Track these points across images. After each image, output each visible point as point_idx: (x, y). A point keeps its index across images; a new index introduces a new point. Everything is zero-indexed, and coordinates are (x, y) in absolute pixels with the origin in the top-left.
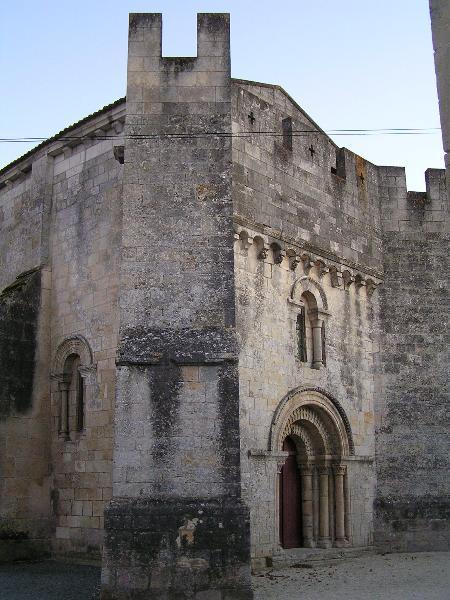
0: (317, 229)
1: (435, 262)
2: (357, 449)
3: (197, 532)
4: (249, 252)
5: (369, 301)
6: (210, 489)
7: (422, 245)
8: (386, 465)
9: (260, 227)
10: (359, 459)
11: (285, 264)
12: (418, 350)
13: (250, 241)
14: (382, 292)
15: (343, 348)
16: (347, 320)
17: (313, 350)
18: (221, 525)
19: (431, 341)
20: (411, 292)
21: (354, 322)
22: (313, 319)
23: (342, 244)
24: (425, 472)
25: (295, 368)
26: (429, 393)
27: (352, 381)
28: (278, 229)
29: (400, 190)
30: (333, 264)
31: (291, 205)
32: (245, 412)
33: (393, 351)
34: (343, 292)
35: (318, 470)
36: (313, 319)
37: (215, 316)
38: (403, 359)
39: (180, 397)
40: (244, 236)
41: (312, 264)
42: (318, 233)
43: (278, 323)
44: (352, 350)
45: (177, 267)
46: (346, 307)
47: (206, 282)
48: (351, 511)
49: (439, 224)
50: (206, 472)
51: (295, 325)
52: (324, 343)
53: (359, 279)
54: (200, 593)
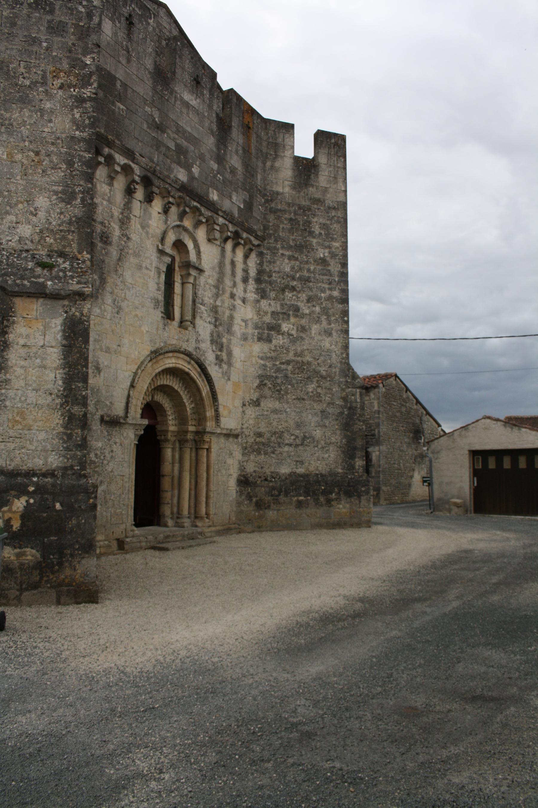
0: (195, 170)
1: (317, 229)
2: (223, 420)
3: (25, 516)
4: (116, 184)
5: (245, 263)
6: (46, 458)
7: (305, 210)
8: (251, 440)
9: (129, 154)
10: (224, 432)
11: (157, 205)
12: (292, 320)
13: (118, 169)
14: (261, 255)
15: (214, 310)
16: (220, 280)
17: (182, 307)
18: (58, 506)
19: (307, 311)
20: (290, 258)
21: (228, 282)
22: (184, 273)
23: (221, 194)
24: (291, 449)
25: (161, 326)
26: (301, 367)
27: (222, 347)
28: (152, 161)
29: (287, 147)
30: (209, 214)
31: (169, 136)
32: (98, 369)
33: (268, 319)
34: (220, 248)
35: (180, 441)
36: (184, 273)
37: (64, 238)
38: (275, 328)
39: (11, 337)
40: (110, 160)
41: (187, 210)
42: (196, 175)
43: (144, 271)
44: (224, 313)
45: (17, 170)
46: (221, 265)
47: (56, 193)
48: (212, 487)
49: (325, 190)
50: (42, 436)
51: (163, 277)
52: (194, 301)
53: (237, 235)
54: (26, 593)
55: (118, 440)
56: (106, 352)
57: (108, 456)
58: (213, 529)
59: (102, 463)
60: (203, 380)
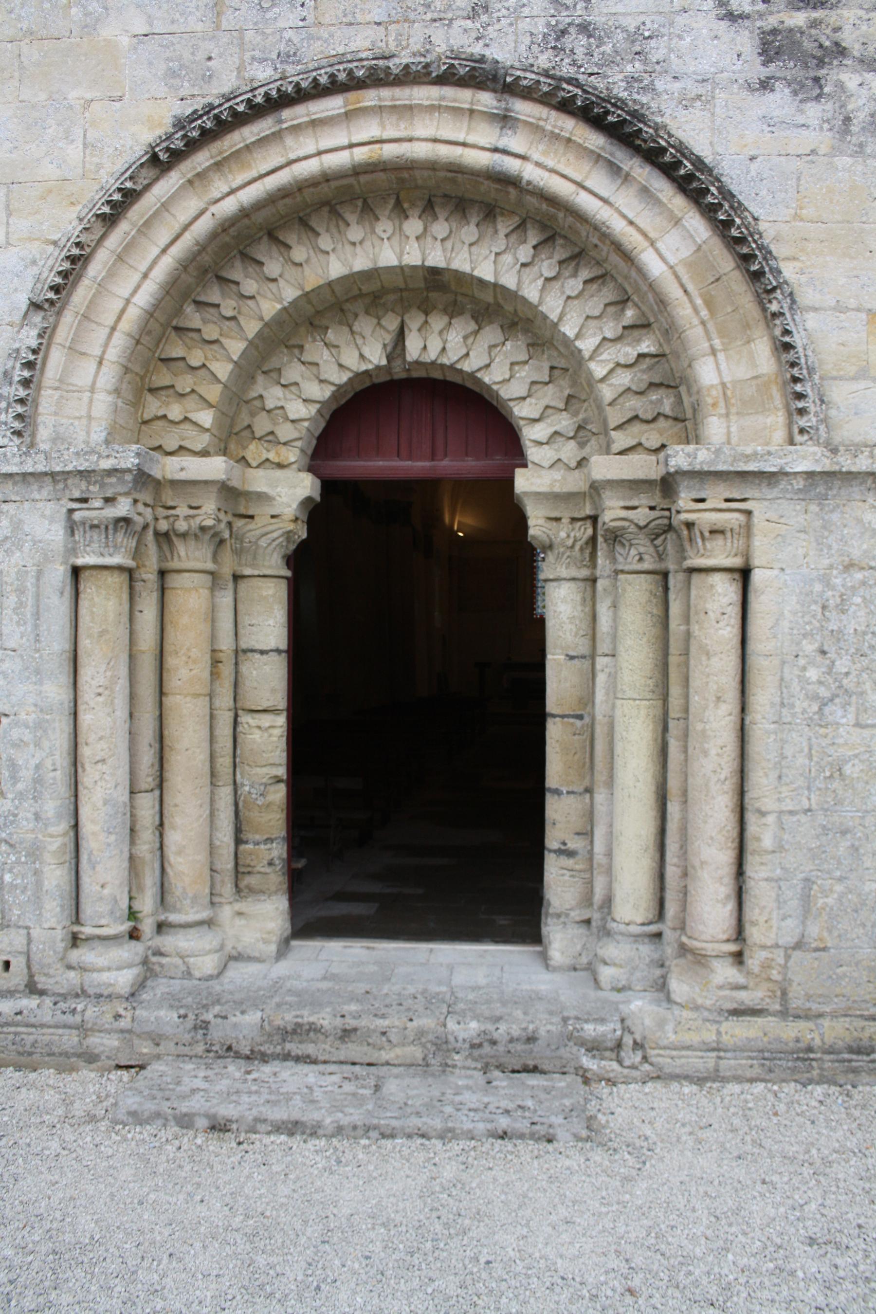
60: (645, 191)
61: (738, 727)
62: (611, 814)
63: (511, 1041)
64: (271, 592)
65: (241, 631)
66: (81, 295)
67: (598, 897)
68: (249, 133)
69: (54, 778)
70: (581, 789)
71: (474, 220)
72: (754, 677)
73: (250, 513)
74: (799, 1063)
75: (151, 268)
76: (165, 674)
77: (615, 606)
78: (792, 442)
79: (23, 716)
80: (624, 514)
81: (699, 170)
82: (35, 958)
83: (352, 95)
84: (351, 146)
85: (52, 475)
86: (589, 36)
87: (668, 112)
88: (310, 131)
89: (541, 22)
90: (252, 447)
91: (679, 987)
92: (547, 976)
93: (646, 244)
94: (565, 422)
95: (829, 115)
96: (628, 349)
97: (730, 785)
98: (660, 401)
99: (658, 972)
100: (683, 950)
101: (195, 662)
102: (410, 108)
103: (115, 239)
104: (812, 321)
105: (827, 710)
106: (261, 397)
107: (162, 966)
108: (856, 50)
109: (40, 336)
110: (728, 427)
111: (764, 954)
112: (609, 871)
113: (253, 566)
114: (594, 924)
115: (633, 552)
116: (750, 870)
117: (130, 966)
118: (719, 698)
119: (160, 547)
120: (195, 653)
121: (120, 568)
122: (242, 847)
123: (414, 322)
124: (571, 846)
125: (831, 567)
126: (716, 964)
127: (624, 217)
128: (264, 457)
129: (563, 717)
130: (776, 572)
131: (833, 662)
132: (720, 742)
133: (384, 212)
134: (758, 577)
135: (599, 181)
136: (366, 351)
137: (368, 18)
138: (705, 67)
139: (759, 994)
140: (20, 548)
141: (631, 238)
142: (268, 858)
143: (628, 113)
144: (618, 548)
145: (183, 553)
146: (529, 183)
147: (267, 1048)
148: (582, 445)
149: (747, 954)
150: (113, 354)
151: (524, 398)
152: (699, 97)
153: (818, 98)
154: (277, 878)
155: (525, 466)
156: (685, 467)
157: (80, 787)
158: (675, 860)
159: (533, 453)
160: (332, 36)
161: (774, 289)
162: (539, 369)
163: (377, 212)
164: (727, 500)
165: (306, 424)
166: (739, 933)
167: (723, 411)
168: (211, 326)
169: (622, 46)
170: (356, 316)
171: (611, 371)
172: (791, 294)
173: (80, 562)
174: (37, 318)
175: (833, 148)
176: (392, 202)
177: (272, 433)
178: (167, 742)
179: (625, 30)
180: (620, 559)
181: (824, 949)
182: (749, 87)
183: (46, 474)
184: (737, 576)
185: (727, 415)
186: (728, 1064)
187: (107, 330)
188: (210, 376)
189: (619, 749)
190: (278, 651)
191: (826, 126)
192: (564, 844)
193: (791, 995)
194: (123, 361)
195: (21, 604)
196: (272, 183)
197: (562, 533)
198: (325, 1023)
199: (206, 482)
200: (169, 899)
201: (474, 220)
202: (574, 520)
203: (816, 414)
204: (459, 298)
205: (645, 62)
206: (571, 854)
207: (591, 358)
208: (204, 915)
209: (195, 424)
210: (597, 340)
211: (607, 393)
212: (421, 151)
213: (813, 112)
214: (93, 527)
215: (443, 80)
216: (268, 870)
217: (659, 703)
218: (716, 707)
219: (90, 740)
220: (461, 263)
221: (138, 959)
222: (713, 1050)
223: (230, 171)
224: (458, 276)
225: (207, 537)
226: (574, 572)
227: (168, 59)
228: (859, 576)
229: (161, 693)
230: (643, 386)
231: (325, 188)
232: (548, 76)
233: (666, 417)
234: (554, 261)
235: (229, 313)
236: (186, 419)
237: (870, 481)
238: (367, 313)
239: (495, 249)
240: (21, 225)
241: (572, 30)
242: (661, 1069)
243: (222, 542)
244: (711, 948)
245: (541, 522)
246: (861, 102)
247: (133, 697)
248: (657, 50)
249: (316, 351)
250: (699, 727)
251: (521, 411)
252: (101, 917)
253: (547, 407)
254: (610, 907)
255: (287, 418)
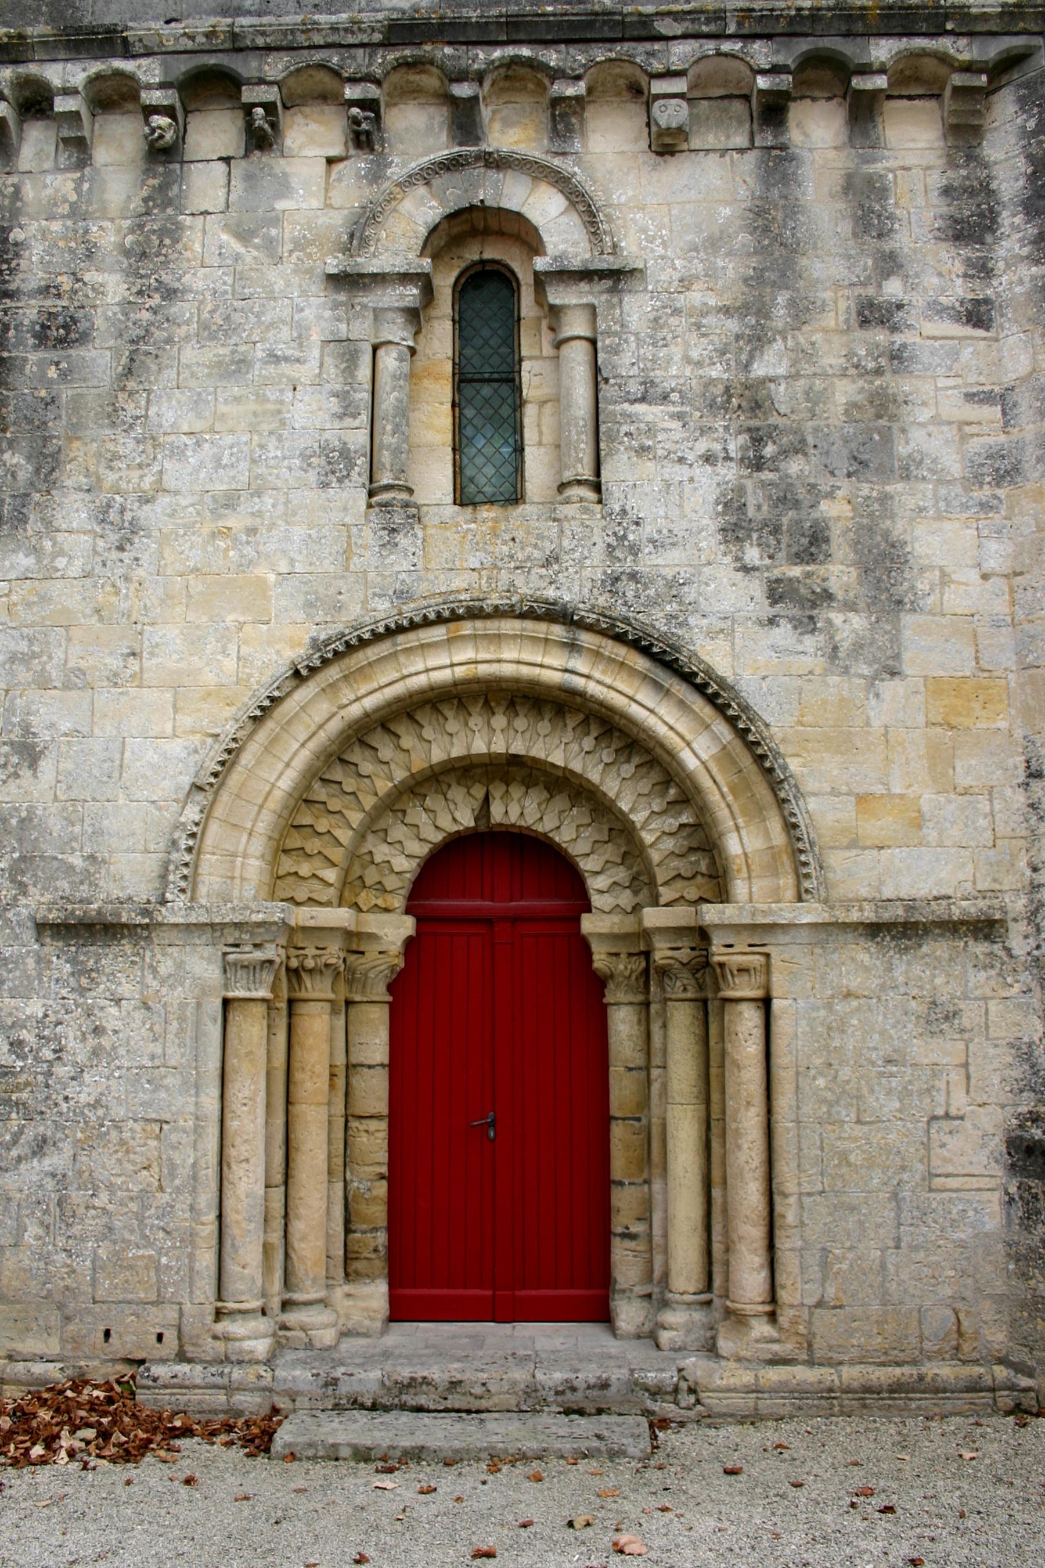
55: (126, 989)
56: (67, 686)
57: (78, 1049)
58: (803, 1374)
59: (49, 1074)
60: (682, 704)
61: (765, 1125)
62: (666, 1201)
63: (589, 1387)
64: (377, 1016)
65: (352, 1049)
66: (235, 779)
67: (657, 1274)
68: (372, 653)
69: (206, 1175)
70: (640, 1180)
71: (547, 716)
72: (776, 1087)
73: (361, 949)
74: (823, 1402)
75: (291, 759)
76: (292, 1087)
77: (664, 1026)
78: (800, 900)
79: (181, 1123)
80: (670, 953)
81: (723, 690)
82: (186, 1329)
83: (452, 625)
84: (452, 665)
85: (212, 926)
86: (637, 583)
87: (699, 642)
88: (420, 652)
89: (599, 571)
90: (363, 894)
91: (725, 1345)
92: (618, 1343)
93: (683, 745)
94: (622, 874)
95: (822, 644)
96: (671, 820)
97: (760, 1172)
98: (697, 862)
99: (709, 1334)
100: (728, 1313)
101: (318, 1076)
102: (499, 636)
103: (263, 735)
104: (812, 804)
105: (834, 1110)
106: (371, 852)
107: (288, 1339)
108: (840, 595)
109: (202, 811)
110: (750, 888)
111: (791, 1312)
112: (666, 1250)
113: (363, 993)
114: (654, 1297)
115: (679, 984)
116: (778, 1244)
117: (265, 1336)
118: (748, 1103)
119: (289, 981)
120: (318, 1068)
121: (263, 1000)
122: (351, 1236)
123: (497, 791)
124: (633, 1229)
125: (833, 997)
126: (754, 1322)
127: (666, 723)
128: (374, 902)
129: (624, 1119)
130: (790, 1001)
131: (837, 1072)
132: (750, 1138)
133: (476, 709)
134: (777, 1004)
135: (646, 695)
136: (458, 815)
137: (465, 565)
138: (726, 606)
139: (789, 1346)
140: (182, 985)
141: (673, 740)
142: (373, 1245)
143: (668, 645)
144: (666, 980)
145: (309, 985)
146: (592, 696)
147: (385, 1400)
148: (636, 893)
149: (779, 1312)
150: (262, 827)
151: (588, 855)
152: (722, 631)
153: (813, 631)
154: (380, 1264)
155: (589, 911)
156: (717, 921)
157: (225, 1183)
158: (720, 1238)
159: (596, 900)
160: (436, 578)
161: (782, 781)
162: (600, 831)
163: (471, 709)
164: (750, 945)
165: (408, 875)
166: (773, 1298)
167: (745, 875)
168: (335, 800)
169: (662, 590)
170: (449, 786)
171: (658, 838)
172: (796, 786)
173: (231, 994)
174: (199, 797)
175: (825, 670)
176: (482, 701)
177: (380, 883)
178: (293, 1144)
179: (664, 578)
180: (669, 989)
181: (840, 1307)
182: (760, 622)
183: (206, 924)
184: (760, 1004)
185: (749, 878)
186: (766, 1404)
187: (256, 808)
188: (332, 840)
189: (670, 1146)
190: (382, 1065)
191: (819, 653)
192: (627, 1228)
193: (815, 1346)
194: (269, 833)
195: (181, 1030)
196: (390, 693)
197: (621, 966)
198: (435, 1377)
199: (332, 929)
200: (293, 1280)
201: (547, 716)
202: (630, 955)
203: (817, 878)
204: (534, 772)
205: (681, 603)
206: (633, 1237)
207: (642, 828)
208: (321, 1294)
209: (322, 880)
210: (647, 813)
211: (655, 856)
212: (508, 670)
213: (810, 642)
214: (243, 967)
215: (522, 616)
216: (373, 1256)
217: (703, 1107)
218: (747, 1110)
219: (236, 1143)
220: (538, 751)
221: (271, 1331)
222: (753, 1392)
223: (356, 681)
224: (534, 760)
225: (330, 971)
226: (631, 998)
227: (307, 593)
228: (855, 1003)
229: (288, 1102)
230: (684, 850)
231: (430, 694)
232: (605, 616)
233: (703, 875)
234: (612, 750)
235: (350, 790)
236: (314, 875)
237: (860, 930)
238: (459, 783)
239: (565, 740)
240: (186, 721)
241: (624, 577)
242: (710, 1409)
243: (339, 973)
244: (750, 1309)
245: (603, 957)
246: (845, 635)
247: (269, 1106)
248: (690, 593)
249: (417, 815)
250: (734, 1126)
251: (586, 865)
252: (243, 1293)
253: (607, 862)
254: (667, 1282)
255: (392, 871)
